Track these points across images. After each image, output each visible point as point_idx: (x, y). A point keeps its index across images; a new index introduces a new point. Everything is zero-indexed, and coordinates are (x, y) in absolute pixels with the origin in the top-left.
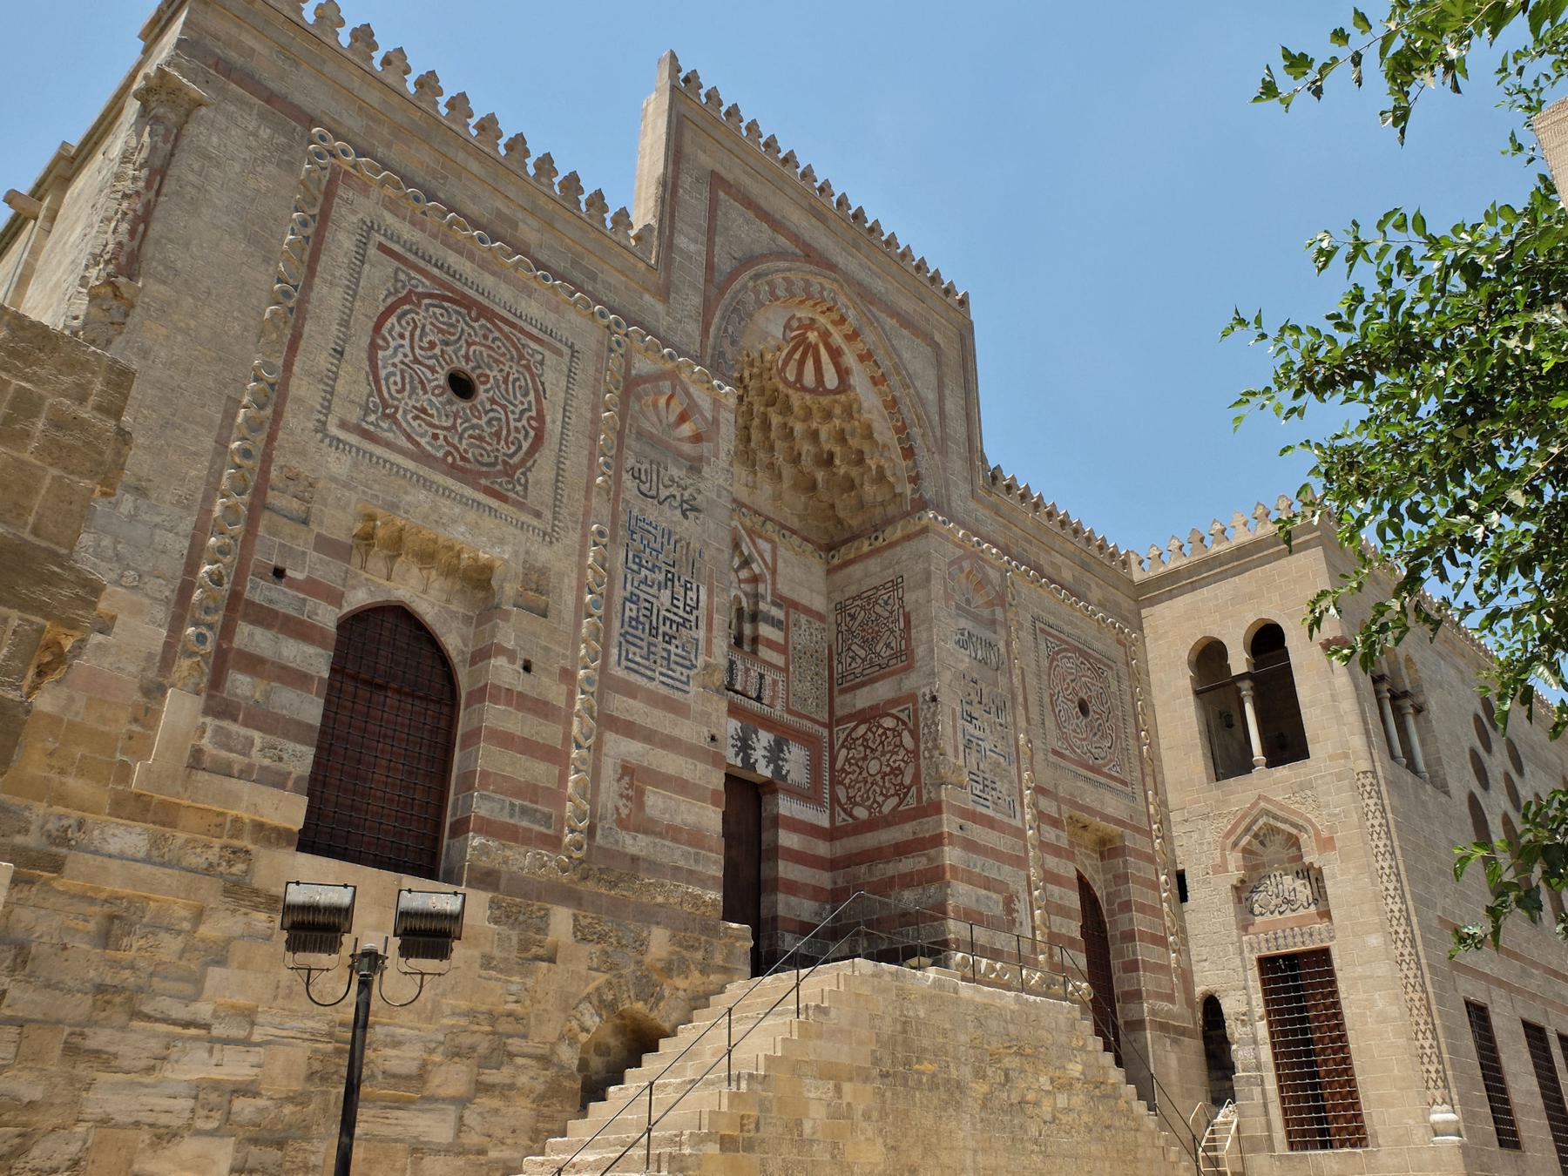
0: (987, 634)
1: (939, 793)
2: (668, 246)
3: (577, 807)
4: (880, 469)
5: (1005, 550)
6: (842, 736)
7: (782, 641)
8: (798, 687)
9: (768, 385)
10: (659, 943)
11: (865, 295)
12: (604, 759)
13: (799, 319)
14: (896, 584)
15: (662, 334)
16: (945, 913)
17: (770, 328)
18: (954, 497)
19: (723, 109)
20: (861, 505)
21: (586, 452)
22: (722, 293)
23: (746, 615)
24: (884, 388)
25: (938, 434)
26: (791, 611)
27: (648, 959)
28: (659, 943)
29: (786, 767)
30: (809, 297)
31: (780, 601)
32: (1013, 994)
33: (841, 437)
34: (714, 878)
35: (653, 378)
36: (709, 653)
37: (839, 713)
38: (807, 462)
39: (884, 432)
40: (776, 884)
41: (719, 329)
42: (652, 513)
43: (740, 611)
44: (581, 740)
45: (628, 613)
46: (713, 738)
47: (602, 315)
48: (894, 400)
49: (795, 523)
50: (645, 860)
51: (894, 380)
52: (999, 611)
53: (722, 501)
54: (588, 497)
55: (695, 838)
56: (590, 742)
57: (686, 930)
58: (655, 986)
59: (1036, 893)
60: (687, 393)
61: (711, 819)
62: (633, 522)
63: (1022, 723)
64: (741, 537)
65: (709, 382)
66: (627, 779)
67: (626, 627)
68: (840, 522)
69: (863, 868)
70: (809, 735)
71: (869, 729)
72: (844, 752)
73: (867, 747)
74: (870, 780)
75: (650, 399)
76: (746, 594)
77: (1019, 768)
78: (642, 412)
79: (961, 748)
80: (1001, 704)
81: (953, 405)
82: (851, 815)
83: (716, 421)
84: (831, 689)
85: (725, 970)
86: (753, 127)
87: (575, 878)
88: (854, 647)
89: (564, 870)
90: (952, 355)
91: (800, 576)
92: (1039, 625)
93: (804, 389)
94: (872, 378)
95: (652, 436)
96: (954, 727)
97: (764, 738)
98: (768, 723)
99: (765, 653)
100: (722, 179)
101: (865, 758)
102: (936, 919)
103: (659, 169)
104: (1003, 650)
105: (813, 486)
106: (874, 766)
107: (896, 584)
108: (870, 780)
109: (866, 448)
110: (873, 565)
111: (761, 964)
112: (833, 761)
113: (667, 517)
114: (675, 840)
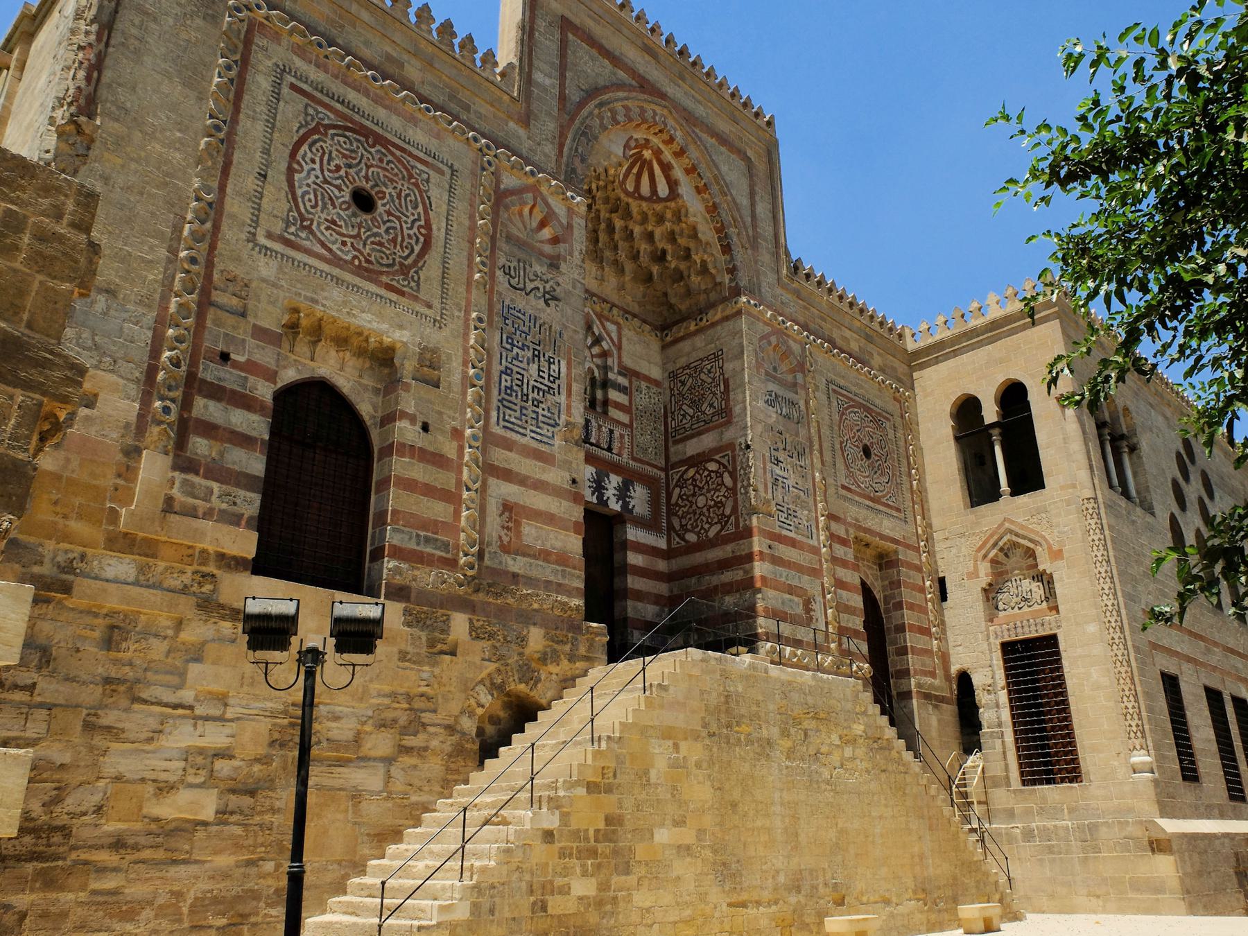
0: (790, 395)
2: (528, 81)
3: (468, 536)
4: (704, 263)
5: (805, 327)
6: (676, 477)
8: (641, 439)
9: (612, 195)
10: (536, 639)
11: (689, 118)
12: (489, 498)
14: (717, 356)
17: (612, 148)
20: (689, 293)
22: (572, 120)
24: (706, 196)
25: (751, 233)
26: (634, 379)
27: (527, 651)
28: (536, 639)
30: (644, 121)
36: (569, 413)
37: (674, 459)
38: (644, 259)
39: (707, 233)
40: (625, 593)
41: (571, 149)
42: (521, 302)
44: (470, 484)
45: (503, 384)
46: (574, 481)
47: (476, 140)
48: (715, 206)
49: (636, 308)
51: (715, 189)
53: (577, 292)
54: (468, 290)
55: (562, 559)
56: (477, 485)
57: (557, 628)
58: (534, 671)
59: (829, 596)
61: (574, 544)
62: (506, 310)
67: (503, 395)
68: (671, 306)
69: (693, 580)
70: (649, 477)
71: (697, 472)
72: (677, 490)
73: (695, 486)
76: (598, 366)
77: (815, 500)
79: (770, 485)
81: (762, 209)
82: (683, 539)
83: (570, 226)
84: (666, 441)
87: (470, 591)
88: (684, 407)
89: (461, 585)
90: (761, 167)
91: (640, 352)
92: (832, 386)
93: (641, 198)
94: (697, 187)
95: (518, 239)
96: (764, 468)
97: (614, 480)
98: (617, 468)
101: (694, 495)
103: (519, 16)
104: (803, 407)
105: (649, 279)
107: (717, 356)
109: (692, 245)
110: (699, 341)
111: (616, 653)
112: (669, 496)
113: (532, 305)
114: (546, 560)
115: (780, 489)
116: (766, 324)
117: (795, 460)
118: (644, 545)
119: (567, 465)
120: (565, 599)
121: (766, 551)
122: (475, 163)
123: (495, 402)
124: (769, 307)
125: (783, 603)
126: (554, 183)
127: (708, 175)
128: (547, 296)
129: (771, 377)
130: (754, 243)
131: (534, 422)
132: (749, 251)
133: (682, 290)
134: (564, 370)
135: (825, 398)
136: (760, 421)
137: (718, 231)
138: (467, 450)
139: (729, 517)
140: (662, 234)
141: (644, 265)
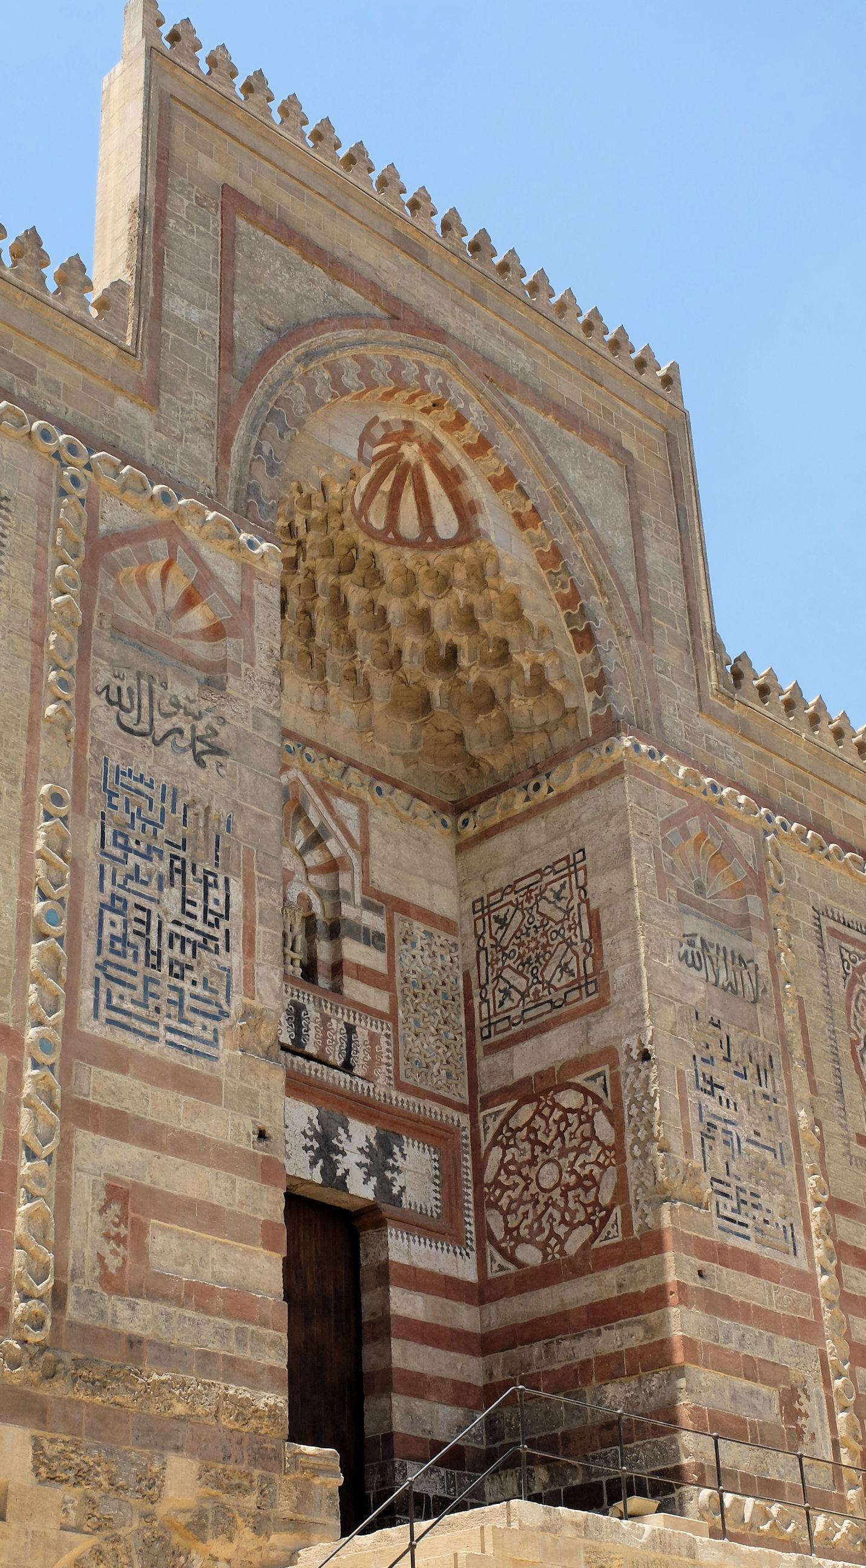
0: (735, 943)
1: (658, 1216)
2: (154, 314)
3: (31, 1255)
4: (538, 671)
5: (762, 798)
6: (494, 1125)
7: (383, 968)
8: (413, 1045)
9: (340, 539)
10: (181, 1482)
11: (496, 377)
12: (76, 1176)
13: (386, 424)
14: (573, 864)
15: (149, 458)
16: (674, 1420)
17: (335, 442)
18: (668, 710)
19: (239, 81)
20: (509, 733)
21: (26, 664)
22: (248, 388)
23: (321, 928)
24: (538, 532)
25: (636, 605)
26: (397, 916)
27: (162, 1509)
28: (181, 1482)
29: (399, 1181)
30: (401, 385)
31: (378, 901)
32: (794, 1556)
33: (469, 620)
34: (272, 1369)
35: (136, 536)
36: (250, 990)
37: (487, 1086)
38: (412, 665)
39: (542, 606)
40: (387, 1380)
41: (246, 447)
42: (142, 759)
43: (310, 922)
44: (35, 1145)
45: (107, 930)
46: (262, 1135)
47: (46, 436)
48: (557, 553)
49: (397, 769)
50: (151, 1343)
51: (555, 517)
52: (754, 904)
53: (263, 735)
54: (32, 737)
55: (238, 1305)
56: (51, 1147)
57: (227, 1458)
58: (177, 1554)
59: (838, 1383)
60: (197, 559)
61: (264, 1271)
62: (111, 777)
63: (803, 1091)
64: (306, 797)
65: (231, 536)
66: (116, 1208)
67: (106, 954)
68: (474, 763)
69: (537, 1349)
70: (437, 1125)
71: (538, 1112)
72: (496, 1153)
73: (535, 1142)
74: (542, 1199)
75: (134, 569)
76: (319, 893)
77: (799, 1169)
78: (119, 592)
79: (696, 1138)
80: (763, 1062)
81: (660, 555)
82: (513, 1260)
83: (247, 602)
84: (471, 1046)
85: (295, 1525)
86: (290, 108)
87: (34, 1376)
88: (507, 974)
89: (15, 1364)
90: (653, 469)
91: (411, 858)
92: (827, 923)
93: (401, 541)
94: (517, 516)
95: (138, 632)
96: (683, 1102)
97: (359, 1134)
98: (365, 1108)
99: (354, 989)
100: (241, 197)
101: (532, 1162)
102: (662, 1432)
103: (133, 189)
104: (764, 968)
105: (426, 705)
106: (548, 1175)
107: (573, 864)
108: (542, 1199)
109: (512, 634)
110: (534, 832)
111: (359, 1510)
112: (479, 1166)
113: (168, 766)
114: (201, 1307)
115: (719, 1147)
116: (675, 791)
117: (750, 1083)
118: (431, 1274)
119: (247, 1099)
120: (245, 1393)
121: (694, 1282)
122: (45, 482)
123: (88, 970)
124: (683, 756)
125: (734, 1398)
126: (211, 515)
127: (539, 491)
128: (200, 746)
129: (692, 903)
130: (643, 626)
131: (174, 1010)
132: (633, 642)
133: (495, 727)
134: (237, 898)
135: (812, 946)
136: (670, 1000)
137: (567, 602)
138: (29, 1072)
139: (609, 1210)
140: (448, 613)
141: (412, 679)
